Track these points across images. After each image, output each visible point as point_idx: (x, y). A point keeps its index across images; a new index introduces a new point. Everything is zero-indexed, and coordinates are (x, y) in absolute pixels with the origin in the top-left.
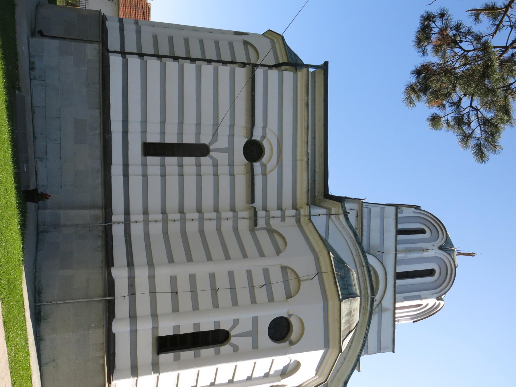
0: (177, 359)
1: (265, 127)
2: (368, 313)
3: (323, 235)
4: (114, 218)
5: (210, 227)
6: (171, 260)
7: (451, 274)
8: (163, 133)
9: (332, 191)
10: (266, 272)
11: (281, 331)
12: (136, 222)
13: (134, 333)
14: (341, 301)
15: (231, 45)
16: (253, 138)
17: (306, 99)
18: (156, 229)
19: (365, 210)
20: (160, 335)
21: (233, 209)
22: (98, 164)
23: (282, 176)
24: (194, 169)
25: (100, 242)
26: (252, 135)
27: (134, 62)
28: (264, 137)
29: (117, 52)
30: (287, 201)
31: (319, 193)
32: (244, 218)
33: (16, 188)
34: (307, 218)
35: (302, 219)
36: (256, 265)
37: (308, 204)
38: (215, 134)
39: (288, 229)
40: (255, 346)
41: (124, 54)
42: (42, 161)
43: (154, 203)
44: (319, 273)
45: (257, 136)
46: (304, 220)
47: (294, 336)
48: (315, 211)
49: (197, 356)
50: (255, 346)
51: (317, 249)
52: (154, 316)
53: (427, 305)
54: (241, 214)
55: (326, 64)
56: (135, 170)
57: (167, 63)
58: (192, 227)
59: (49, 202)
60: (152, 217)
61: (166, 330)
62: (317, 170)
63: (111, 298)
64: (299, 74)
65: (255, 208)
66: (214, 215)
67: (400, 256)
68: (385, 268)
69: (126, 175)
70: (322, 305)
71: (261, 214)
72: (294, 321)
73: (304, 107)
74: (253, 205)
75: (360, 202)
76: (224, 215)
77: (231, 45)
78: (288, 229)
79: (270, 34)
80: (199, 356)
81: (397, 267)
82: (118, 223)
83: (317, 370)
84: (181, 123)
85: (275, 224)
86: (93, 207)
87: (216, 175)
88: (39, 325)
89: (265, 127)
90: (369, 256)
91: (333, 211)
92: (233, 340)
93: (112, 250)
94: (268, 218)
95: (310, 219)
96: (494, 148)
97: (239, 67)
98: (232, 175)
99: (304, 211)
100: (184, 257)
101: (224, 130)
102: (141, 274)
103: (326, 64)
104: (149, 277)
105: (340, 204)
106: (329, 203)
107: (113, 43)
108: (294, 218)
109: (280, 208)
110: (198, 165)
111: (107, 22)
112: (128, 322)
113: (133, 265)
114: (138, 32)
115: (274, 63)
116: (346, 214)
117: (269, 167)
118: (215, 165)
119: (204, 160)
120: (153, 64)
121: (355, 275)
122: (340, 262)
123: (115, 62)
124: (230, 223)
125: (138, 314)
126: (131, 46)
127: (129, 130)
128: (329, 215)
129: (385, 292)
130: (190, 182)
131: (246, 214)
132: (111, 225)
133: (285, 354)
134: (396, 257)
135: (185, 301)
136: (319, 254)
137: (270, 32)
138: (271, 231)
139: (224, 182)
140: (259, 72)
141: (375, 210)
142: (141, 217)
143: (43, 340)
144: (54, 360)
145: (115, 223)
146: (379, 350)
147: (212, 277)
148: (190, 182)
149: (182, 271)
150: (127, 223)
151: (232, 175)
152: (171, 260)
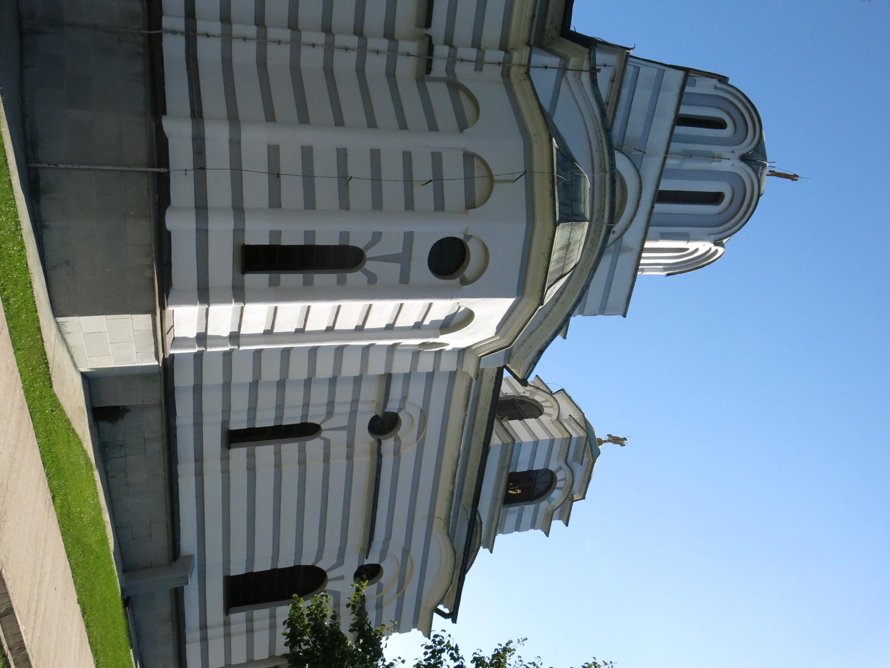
0: (274, 284)
2: (597, 251)
7: (749, 206)
9: (580, 24)
10: (437, 158)
11: (450, 263)
13: (202, 234)
14: (556, 225)
18: (244, 54)
19: (630, 69)
25: (139, 66)
26: (385, 406)
30: (492, 32)
34: (523, 70)
36: (422, 144)
37: (528, 44)
40: (405, 279)
44: (528, 172)
47: (469, 271)
48: (540, 58)
49: (308, 283)
50: (405, 279)
52: (238, 210)
53: (697, 250)
61: (258, 234)
63: (162, 170)
65: (430, 37)
68: (639, 180)
71: (441, 50)
72: (472, 245)
78: (486, 86)
81: (662, 181)
82: (174, 32)
85: (464, 73)
88: (38, 202)
90: (618, 156)
91: (573, 63)
92: (369, 265)
93: (163, 84)
94: (452, 60)
95: (527, 73)
99: (519, 56)
102: (217, 135)
105: (586, 50)
106: (569, 46)
108: (500, 68)
109: (476, 44)
112: (193, 214)
113: (201, 116)
116: (593, 72)
121: (588, 185)
122: (567, 159)
127: (210, 286)
132: (160, 36)
135: (292, 190)
138: (454, 86)
141: (648, 73)
142: (216, 27)
144: (68, 263)
145: (167, 31)
149: (291, 139)
150: (191, 35)
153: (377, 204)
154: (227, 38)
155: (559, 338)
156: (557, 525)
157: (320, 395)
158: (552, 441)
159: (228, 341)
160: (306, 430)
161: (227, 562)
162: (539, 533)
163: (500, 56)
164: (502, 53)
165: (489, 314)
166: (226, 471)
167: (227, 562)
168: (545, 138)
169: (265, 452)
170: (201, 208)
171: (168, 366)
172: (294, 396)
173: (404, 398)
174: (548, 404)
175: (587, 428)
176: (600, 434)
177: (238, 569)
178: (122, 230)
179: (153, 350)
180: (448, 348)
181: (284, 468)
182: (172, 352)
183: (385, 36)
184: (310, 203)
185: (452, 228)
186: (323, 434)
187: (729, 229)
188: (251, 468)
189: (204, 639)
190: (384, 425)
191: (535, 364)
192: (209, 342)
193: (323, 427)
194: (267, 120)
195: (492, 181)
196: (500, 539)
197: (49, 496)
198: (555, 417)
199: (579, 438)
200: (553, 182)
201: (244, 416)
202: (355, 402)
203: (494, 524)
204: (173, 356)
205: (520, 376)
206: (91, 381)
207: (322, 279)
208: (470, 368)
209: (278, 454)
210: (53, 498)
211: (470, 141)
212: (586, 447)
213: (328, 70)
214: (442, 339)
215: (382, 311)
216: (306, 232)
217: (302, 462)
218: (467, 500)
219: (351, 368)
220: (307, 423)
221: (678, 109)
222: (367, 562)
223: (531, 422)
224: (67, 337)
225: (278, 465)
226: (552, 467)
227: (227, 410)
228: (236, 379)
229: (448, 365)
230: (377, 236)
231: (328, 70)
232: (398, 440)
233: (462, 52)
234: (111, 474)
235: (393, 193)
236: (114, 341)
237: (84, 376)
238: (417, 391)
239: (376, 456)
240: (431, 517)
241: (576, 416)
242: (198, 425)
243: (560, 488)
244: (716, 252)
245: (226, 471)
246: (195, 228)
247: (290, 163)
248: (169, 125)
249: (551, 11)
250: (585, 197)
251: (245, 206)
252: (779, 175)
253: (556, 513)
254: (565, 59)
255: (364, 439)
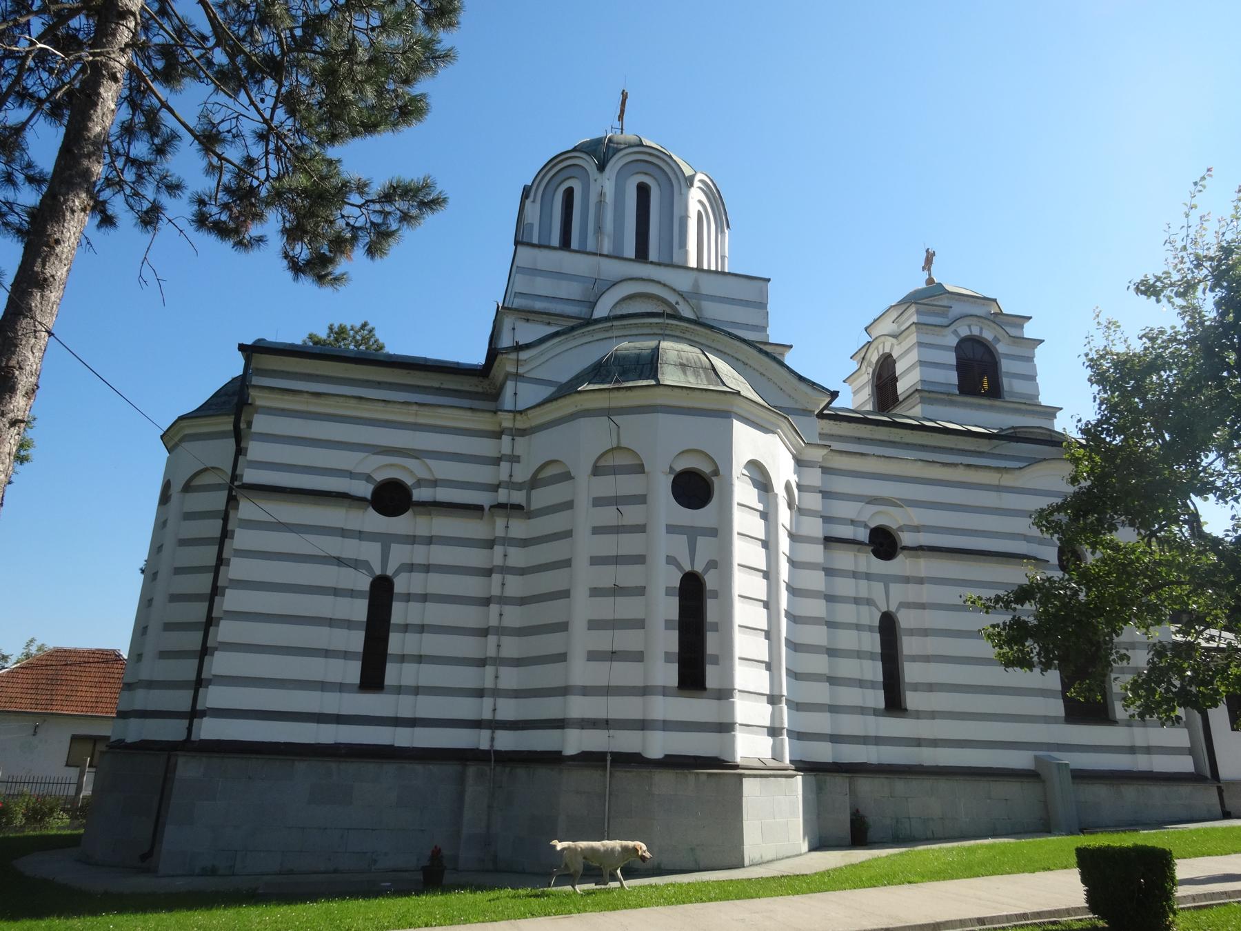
0: (716, 660)
1: (351, 475)
2: (693, 327)
3: (547, 391)
4: (484, 745)
5: (515, 586)
6: (562, 657)
7: (650, 154)
8: (346, 655)
9: (476, 356)
10: (598, 502)
11: (696, 488)
12: (495, 710)
13: (667, 726)
14: (658, 385)
15: (189, 516)
16: (369, 496)
17: (306, 396)
18: (510, 678)
19: (518, 303)
20: (358, 681)
21: (490, 544)
22: (390, 769)
23: (440, 450)
24: (414, 606)
25: (521, 772)
26: (362, 499)
27: (214, 697)
28: (368, 478)
29: (191, 725)
30: (485, 447)
31: (477, 384)
32: (507, 527)
33: (417, 894)
34: (518, 417)
35: (519, 425)
36: (585, 517)
37: (495, 412)
38: (356, 564)
39: (534, 452)
40: (713, 532)
41: (194, 714)
42: (375, 861)
43: (466, 677)
44: (608, 412)
45: (365, 489)
46: (521, 423)
47: (706, 468)
48: (507, 401)
49: (715, 627)
50: (713, 532)
51: (572, 409)
52: (645, 691)
53: (700, 202)
54: (499, 531)
55: (242, 348)
56: (405, 706)
57: (220, 639)
58: (514, 616)
59: (446, 852)
60: (489, 684)
61: (669, 674)
62: (436, 384)
63: (609, 758)
64: (258, 402)
65: (492, 507)
66: (496, 577)
67: (607, 248)
68: (624, 280)
69: (413, 722)
70: (661, 417)
71: (503, 496)
72: (680, 466)
73: (322, 401)
74: (487, 507)
75: (502, 312)
76: (498, 560)
77: (189, 516)
78: (533, 452)
79: (173, 437)
80: (716, 624)
81: (626, 255)
82: (492, 739)
83: (766, 430)
84: (331, 622)
85: (522, 473)
86: (461, 780)
87: (427, 568)
88: (637, 870)
89: (351, 475)
90: (599, 312)
91: (511, 368)
92: (699, 568)
93: (535, 752)
94: (511, 485)
95: (521, 412)
96: (426, 186)
97: (237, 508)
98: (429, 540)
99: (507, 421)
100: (558, 636)
101: (350, 548)
102: (578, 707)
103: (242, 348)
104: (584, 695)
105: (499, 357)
106: (497, 372)
107: (172, 731)
108: (517, 438)
109: (496, 461)
110: (408, 597)
111: (129, 740)
112: (648, 733)
113: (563, 721)
114: (151, 685)
115: (233, 441)
116: (518, 348)
117: (424, 474)
118: (411, 568)
119: (400, 586)
120: (220, 663)
121: (625, 344)
122: (598, 372)
123: (209, 729)
124: (512, 551)
125: (639, 716)
126: (181, 700)
127: (336, 712)
128: (517, 377)
129: (665, 285)
130: (434, 613)
131: (500, 522)
132: (497, 752)
133: (731, 485)
134: (606, 256)
135: (628, 640)
136: (579, 408)
137: (166, 438)
138: (534, 483)
139: (440, 555)
140: (250, 476)
141: (521, 285)
142: (488, 702)
143: (659, 864)
144: (692, 849)
145: (492, 746)
146: (762, 305)
147: (595, 592)
148: (434, 613)
149: (581, 640)
150: (495, 725)
151: (429, 540)
152: (562, 657)
153: (640, 559)
154: (496, 693)
155: (789, 359)
156: (1029, 331)
157: (846, 613)
158: (920, 344)
159: (777, 707)
160: (888, 627)
161: (1047, 720)
162: (1039, 351)
163: (506, 439)
164: (504, 437)
165: (747, 443)
166: (933, 715)
167: (1047, 720)
168: (578, 397)
169: (911, 672)
170: (643, 725)
171: (804, 767)
172: (847, 639)
173: (853, 522)
174: (881, 347)
175: (913, 299)
176: (918, 282)
177: (1057, 707)
178: (672, 805)
179: (784, 779)
180: (794, 479)
181: (930, 652)
182: (787, 761)
183: (492, 548)
184: (639, 624)
185: (664, 485)
186: (893, 609)
187: (675, 173)
188: (931, 687)
189: (1148, 750)
190: (883, 543)
191: (814, 384)
192: (777, 725)
193: (884, 609)
194: (565, 660)
195: (619, 448)
196: (1045, 400)
197: (906, 886)
198: (894, 340)
199: (918, 312)
200: (618, 389)
201: (870, 693)
202: (855, 575)
203: (1023, 407)
204: (791, 762)
205: (828, 400)
206: (820, 844)
207: (711, 614)
208: (817, 454)
209: (914, 659)
210: (910, 883)
211: (582, 470)
212: (930, 301)
213: (522, 601)
214: (779, 489)
215: (746, 552)
216: (666, 628)
217: (925, 632)
218: (984, 445)
219: (816, 581)
220: (880, 627)
221: (554, 248)
222: (1054, 560)
223: (899, 368)
224: (766, 858)
225: (927, 659)
226: (953, 341)
227: (862, 711)
228: (825, 699)
229: (815, 477)
230: (671, 560)
231: (522, 601)
232: (901, 529)
233: (504, 476)
234: (929, 834)
235: (629, 544)
236: (774, 819)
237: (813, 848)
238: (844, 509)
239: (920, 553)
240: (999, 488)
241: (894, 314)
242: (878, 741)
243: (981, 329)
244: (702, 181)
245: (933, 715)
246: (661, 733)
247: (604, 641)
248: (570, 750)
249: (466, 388)
250: (636, 348)
251: (641, 684)
252: (622, 111)
253: (1013, 332)
254: (508, 376)
255: (900, 565)
